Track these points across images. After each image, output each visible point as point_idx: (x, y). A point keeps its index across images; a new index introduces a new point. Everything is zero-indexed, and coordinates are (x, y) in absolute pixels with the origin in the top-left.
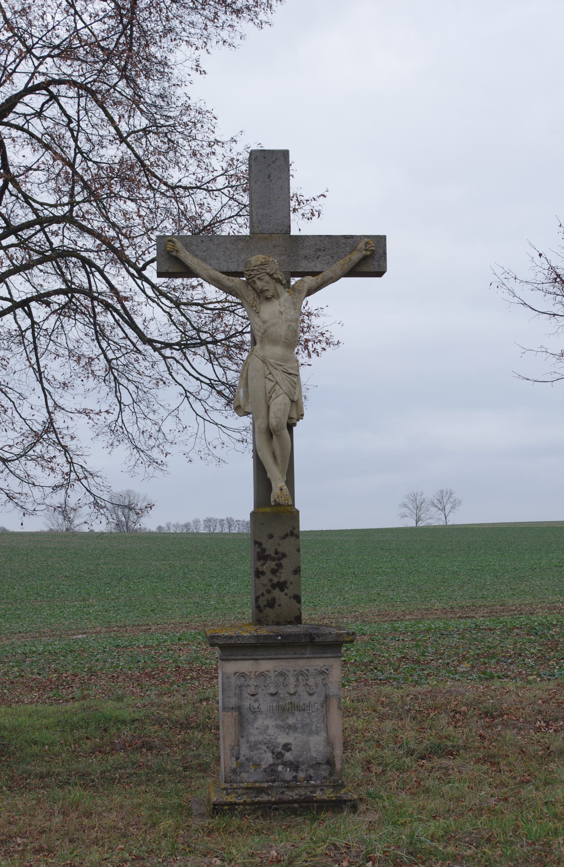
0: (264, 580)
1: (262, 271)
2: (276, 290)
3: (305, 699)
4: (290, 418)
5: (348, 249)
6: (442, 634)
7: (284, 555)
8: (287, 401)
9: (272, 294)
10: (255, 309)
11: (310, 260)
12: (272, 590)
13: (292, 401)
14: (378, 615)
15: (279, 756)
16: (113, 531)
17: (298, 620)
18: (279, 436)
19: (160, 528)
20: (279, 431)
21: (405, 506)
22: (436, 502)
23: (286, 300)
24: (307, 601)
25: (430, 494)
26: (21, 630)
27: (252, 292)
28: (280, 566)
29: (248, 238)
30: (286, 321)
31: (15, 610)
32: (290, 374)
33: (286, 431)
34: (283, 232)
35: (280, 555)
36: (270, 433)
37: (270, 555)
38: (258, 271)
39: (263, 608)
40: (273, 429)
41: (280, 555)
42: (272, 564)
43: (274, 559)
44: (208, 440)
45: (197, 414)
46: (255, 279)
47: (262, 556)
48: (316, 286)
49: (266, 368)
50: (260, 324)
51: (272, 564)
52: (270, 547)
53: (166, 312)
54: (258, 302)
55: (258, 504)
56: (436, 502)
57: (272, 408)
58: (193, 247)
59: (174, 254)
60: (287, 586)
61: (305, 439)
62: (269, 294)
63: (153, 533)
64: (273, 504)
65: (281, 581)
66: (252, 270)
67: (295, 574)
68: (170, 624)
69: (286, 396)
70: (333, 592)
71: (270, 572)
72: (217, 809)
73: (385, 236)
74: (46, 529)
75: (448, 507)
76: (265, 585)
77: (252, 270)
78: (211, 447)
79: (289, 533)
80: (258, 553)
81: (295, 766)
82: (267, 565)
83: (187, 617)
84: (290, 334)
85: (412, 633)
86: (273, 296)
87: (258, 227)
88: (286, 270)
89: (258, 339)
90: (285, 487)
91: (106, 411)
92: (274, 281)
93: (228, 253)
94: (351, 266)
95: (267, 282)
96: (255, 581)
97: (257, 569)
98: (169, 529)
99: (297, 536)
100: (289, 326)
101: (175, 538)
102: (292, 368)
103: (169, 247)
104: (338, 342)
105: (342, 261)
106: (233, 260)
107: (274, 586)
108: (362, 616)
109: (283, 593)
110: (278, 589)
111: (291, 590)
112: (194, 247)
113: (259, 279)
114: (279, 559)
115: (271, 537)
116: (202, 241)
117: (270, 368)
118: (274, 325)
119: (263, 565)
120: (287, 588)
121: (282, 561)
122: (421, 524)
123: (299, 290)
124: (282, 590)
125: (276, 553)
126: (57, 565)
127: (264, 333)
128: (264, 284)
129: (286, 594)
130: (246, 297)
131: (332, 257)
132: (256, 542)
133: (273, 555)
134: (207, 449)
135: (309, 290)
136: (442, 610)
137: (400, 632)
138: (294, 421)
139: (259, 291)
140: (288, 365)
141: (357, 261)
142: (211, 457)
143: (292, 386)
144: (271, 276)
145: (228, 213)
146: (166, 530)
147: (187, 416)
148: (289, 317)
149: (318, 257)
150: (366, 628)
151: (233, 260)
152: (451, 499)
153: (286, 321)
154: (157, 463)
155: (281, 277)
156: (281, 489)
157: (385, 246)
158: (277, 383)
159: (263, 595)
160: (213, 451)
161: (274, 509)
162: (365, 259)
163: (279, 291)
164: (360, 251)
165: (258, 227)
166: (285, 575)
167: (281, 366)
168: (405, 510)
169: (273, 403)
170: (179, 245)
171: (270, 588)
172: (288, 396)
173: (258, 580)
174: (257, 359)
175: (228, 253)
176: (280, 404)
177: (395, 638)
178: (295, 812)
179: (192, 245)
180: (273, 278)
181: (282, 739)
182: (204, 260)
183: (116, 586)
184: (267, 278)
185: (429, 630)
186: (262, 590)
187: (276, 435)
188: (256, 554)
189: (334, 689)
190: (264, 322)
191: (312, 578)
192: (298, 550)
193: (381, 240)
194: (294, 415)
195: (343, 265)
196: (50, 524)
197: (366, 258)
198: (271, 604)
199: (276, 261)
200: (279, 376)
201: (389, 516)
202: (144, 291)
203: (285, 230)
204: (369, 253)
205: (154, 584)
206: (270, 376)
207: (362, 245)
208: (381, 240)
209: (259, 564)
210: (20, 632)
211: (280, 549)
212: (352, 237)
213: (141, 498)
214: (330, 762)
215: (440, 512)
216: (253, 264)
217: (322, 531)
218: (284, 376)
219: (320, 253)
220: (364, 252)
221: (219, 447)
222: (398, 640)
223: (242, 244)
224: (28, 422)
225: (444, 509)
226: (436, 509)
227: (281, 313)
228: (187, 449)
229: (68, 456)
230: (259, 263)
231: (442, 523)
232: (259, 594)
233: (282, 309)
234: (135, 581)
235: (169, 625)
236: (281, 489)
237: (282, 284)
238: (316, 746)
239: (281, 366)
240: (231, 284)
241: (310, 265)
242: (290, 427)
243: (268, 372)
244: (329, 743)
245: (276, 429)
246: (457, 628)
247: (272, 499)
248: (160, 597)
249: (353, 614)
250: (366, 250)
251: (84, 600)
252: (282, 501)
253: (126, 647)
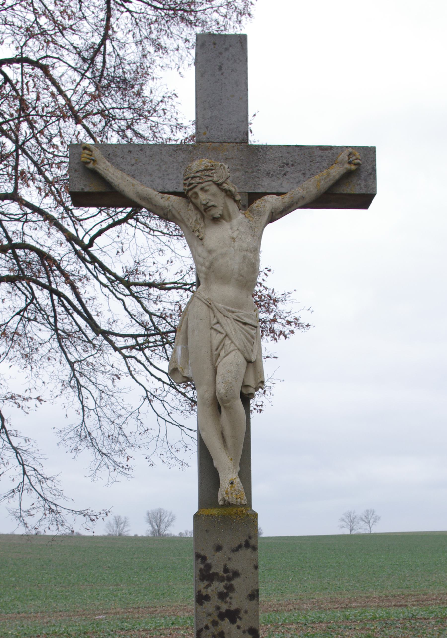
0: (209, 607)
1: (206, 178)
2: (226, 207)
4: (245, 386)
5: (325, 164)
6: (387, 623)
7: (236, 574)
8: (241, 360)
9: (220, 212)
10: (197, 234)
11: (274, 177)
12: (219, 621)
13: (249, 362)
14: (330, 602)
16: (150, 535)
18: (229, 409)
19: (181, 534)
20: (229, 401)
21: (343, 520)
22: (364, 517)
23: (240, 223)
24: (277, 589)
25: (360, 513)
26: (61, 610)
27: (195, 212)
28: (230, 588)
29: (191, 148)
30: (241, 250)
31: (66, 592)
32: (245, 324)
33: (239, 402)
34: (238, 140)
35: (230, 574)
36: (217, 406)
37: (217, 574)
38: (201, 178)
40: (222, 399)
41: (230, 574)
42: (219, 586)
43: (222, 579)
44: (171, 442)
45: (158, 416)
46: (197, 190)
47: (206, 575)
48: (281, 208)
49: (212, 315)
50: (205, 254)
51: (219, 586)
52: (217, 563)
53: (119, 299)
54: (202, 225)
55: (202, 504)
56: (364, 517)
57: (220, 370)
58: (118, 159)
59: (91, 166)
60: (240, 616)
61: (267, 420)
62: (217, 212)
63: (176, 537)
64: (221, 503)
65: (233, 608)
66: (193, 178)
67: (251, 600)
68: (172, 606)
69: (239, 353)
70: (296, 581)
71: (216, 597)
73: (374, 148)
74: (106, 534)
75: (371, 521)
76: (210, 615)
77: (193, 178)
78: (173, 450)
79: (243, 543)
80: (201, 570)
82: (213, 587)
83: (186, 601)
84: (246, 269)
85: (361, 621)
86: (222, 217)
87: (205, 134)
88: (242, 190)
89: (202, 281)
90: (238, 480)
91: (38, 398)
92: (223, 194)
93: (164, 167)
94: (330, 183)
95: (214, 195)
96: (197, 608)
97: (199, 592)
98: (187, 534)
99: (254, 548)
100: (244, 257)
101: (188, 541)
102: (248, 316)
103: (85, 156)
104: (308, 326)
105: (317, 177)
106: (171, 176)
107: (222, 616)
108: (318, 602)
109: (235, 625)
110: (227, 620)
111: (245, 622)
112: (119, 160)
113: (202, 189)
114: (229, 579)
115: (219, 548)
116: (130, 152)
117: (218, 315)
118: (223, 255)
119: (207, 587)
120: (240, 619)
121: (233, 582)
122: (354, 532)
123: (259, 211)
124: (233, 621)
125: (226, 570)
126: (104, 559)
127: (209, 267)
128: (209, 197)
129: (239, 627)
130: (186, 220)
131: (304, 174)
132: (198, 556)
133: (221, 573)
134: (169, 452)
135: (272, 213)
136: (379, 598)
137: (351, 620)
138: (251, 390)
139: (202, 208)
140: (244, 312)
141: (337, 177)
142: (173, 460)
143: (249, 341)
144: (219, 185)
146: (185, 535)
147: (149, 419)
148: (245, 245)
149: (285, 174)
150: (323, 615)
151: (171, 176)
152: (374, 516)
153: (241, 250)
154: (123, 467)
155: (233, 189)
156: (232, 483)
157: (375, 160)
158: (227, 335)
159: (207, 627)
160: (176, 454)
161: (225, 510)
162: (348, 175)
163: (231, 210)
164: (342, 163)
165: (205, 134)
166: (237, 601)
167: (233, 312)
168: (343, 523)
169: (221, 363)
170: (97, 154)
171: (217, 619)
172: (243, 353)
173: (200, 608)
174: (200, 303)
175: (164, 167)
176: (230, 365)
177: (348, 626)
179: (116, 156)
180: (223, 190)
182: (134, 177)
183: (142, 575)
184: (214, 189)
185: (374, 619)
186: (206, 621)
187: (225, 407)
188: (198, 572)
190: (210, 252)
191: (280, 570)
192: (256, 567)
193: (369, 153)
194: (251, 382)
195: (319, 181)
196: (108, 531)
197: (346, 181)
199: (226, 166)
200: (230, 326)
201: (333, 527)
202: (97, 278)
203: (241, 138)
204: (353, 167)
205: (169, 573)
206: (217, 327)
207: (344, 156)
208: (369, 153)
209: (202, 585)
210: (60, 611)
211: (232, 566)
212: (330, 148)
213: (168, 514)
215: (366, 524)
216: (195, 169)
217: (288, 537)
218: (238, 326)
219: (286, 169)
220: (347, 166)
221: (182, 450)
222: (351, 629)
223: (183, 156)
225: (369, 523)
226: (364, 522)
227: (234, 239)
228: (149, 453)
229: (19, 458)
230: (203, 167)
231: (367, 532)
232: (202, 626)
233: (235, 234)
234: (156, 571)
235: (171, 608)
236: (232, 483)
237: (235, 201)
239: (233, 312)
240: (166, 203)
241: (274, 184)
242: (246, 399)
243: (215, 321)
245: (225, 398)
246: (397, 617)
247: (220, 497)
248: (171, 583)
249: (311, 600)
250: (350, 163)
251: (117, 585)
252: (232, 499)
253: (128, 630)
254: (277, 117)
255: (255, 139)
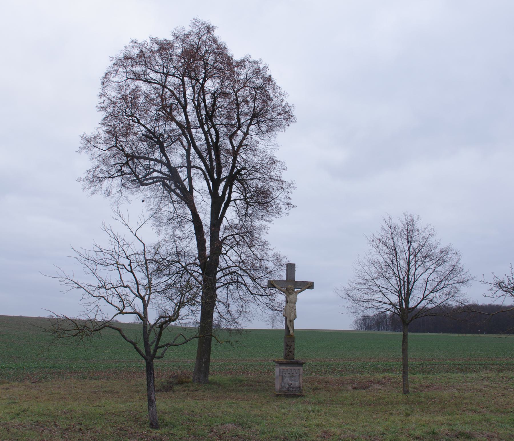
3: (295, 374)
15: (290, 386)
17: (294, 359)
39: (286, 356)
47: (287, 346)
72: (277, 395)
81: (293, 388)
122: (274, 328)
145: (283, 275)
166: (291, 350)
176: (292, 315)
178: (293, 397)
181: (290, 382)
189: (301, 373)
193: (313, 283)
197: (310, 286)
198: (289, 355)
200: (293, 310)
208: (313, 283)
214: (300, 387)
224: (76, 285)
238: (297, 384)
244: (300, 384)
254: (299, 277)
255: (297, 279)
